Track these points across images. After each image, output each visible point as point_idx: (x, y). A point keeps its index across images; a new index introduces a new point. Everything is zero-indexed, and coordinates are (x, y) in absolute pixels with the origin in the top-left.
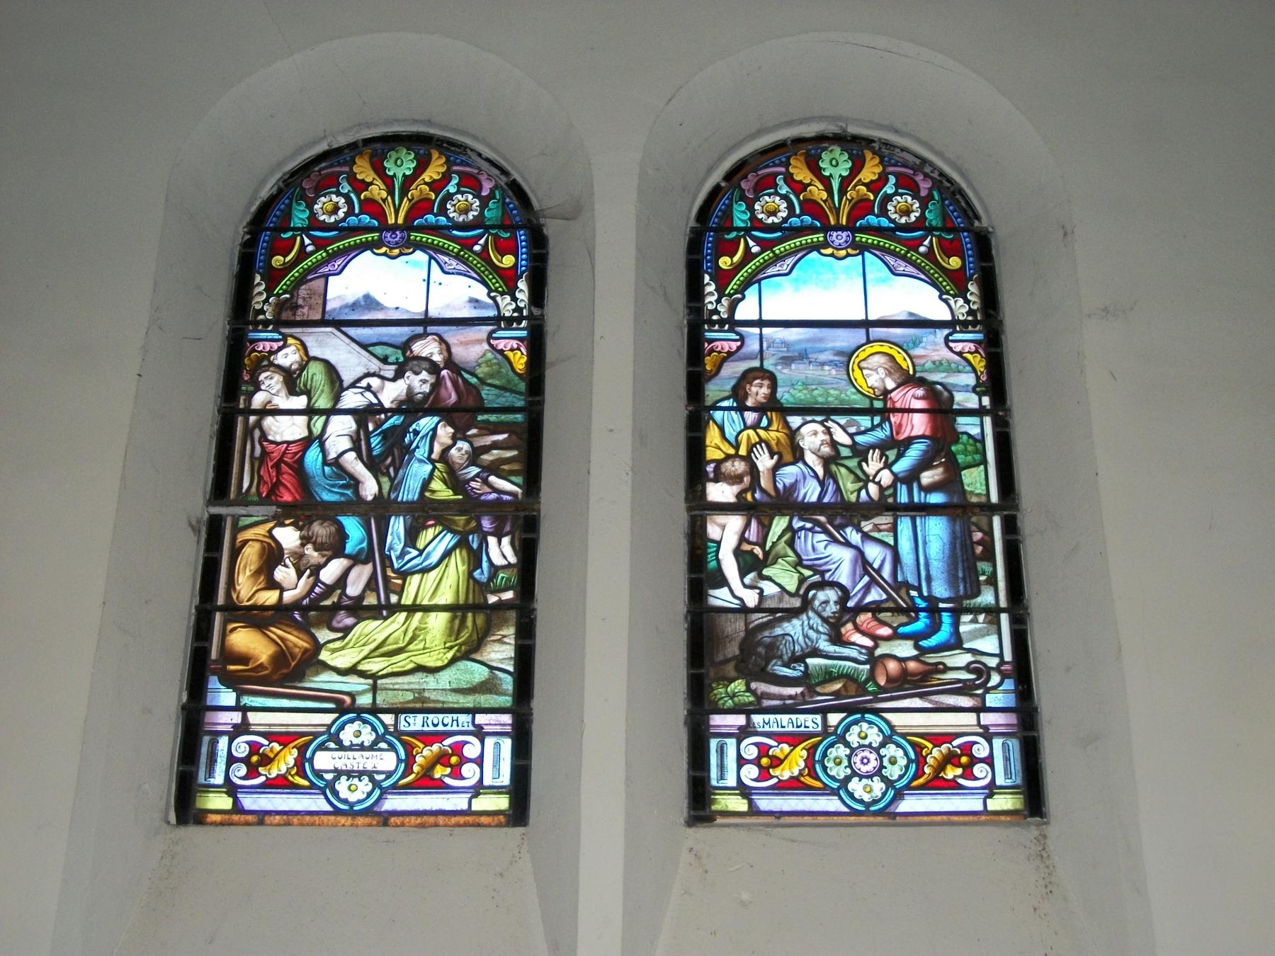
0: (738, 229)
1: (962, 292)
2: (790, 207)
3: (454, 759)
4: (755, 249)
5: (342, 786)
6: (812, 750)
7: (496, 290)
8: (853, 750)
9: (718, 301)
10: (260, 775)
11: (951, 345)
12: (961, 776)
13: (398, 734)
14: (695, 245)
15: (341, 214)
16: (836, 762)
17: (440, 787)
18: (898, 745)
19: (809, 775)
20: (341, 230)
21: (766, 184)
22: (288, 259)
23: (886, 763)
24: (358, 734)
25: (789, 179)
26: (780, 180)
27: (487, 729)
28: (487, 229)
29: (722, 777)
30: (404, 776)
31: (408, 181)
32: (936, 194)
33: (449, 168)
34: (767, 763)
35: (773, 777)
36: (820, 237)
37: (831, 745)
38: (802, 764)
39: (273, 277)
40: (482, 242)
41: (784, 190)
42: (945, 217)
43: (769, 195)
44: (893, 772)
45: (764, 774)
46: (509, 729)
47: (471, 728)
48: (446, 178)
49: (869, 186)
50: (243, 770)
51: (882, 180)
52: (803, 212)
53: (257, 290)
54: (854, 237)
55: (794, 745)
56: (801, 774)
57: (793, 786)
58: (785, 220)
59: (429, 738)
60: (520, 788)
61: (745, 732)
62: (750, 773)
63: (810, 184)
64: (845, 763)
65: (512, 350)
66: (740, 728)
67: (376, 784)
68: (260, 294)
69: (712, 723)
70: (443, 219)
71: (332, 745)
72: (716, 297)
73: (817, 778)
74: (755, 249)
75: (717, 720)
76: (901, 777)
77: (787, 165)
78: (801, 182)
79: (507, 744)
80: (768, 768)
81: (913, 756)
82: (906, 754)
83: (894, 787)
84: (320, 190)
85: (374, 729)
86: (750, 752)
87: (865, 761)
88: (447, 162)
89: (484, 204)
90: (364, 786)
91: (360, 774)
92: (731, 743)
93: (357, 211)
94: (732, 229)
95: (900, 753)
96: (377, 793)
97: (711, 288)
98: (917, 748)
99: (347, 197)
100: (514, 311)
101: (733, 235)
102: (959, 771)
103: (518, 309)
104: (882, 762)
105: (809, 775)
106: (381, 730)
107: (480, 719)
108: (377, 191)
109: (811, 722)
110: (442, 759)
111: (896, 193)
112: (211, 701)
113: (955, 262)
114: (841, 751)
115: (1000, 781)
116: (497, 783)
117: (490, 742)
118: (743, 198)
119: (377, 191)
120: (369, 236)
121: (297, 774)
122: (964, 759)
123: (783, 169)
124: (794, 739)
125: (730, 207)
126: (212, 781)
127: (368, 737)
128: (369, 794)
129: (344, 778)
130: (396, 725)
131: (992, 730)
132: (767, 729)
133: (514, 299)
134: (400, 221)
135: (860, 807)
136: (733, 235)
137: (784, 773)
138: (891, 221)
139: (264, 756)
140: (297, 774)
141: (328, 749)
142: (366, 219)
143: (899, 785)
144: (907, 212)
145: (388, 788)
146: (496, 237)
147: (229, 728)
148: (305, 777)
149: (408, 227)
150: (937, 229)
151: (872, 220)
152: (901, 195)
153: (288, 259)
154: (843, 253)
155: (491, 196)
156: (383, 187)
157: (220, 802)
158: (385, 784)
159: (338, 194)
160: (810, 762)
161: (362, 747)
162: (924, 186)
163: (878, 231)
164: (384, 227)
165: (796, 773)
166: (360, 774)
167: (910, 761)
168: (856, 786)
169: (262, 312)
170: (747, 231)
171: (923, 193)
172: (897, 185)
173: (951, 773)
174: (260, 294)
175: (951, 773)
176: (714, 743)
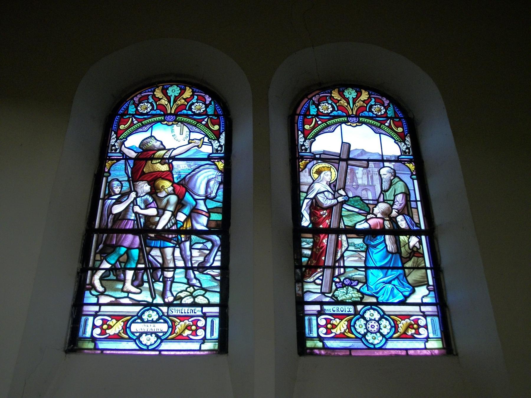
0: (130, 114)
1: (404, 141)
4: (135, 122)
6: (349, 321)
7: (212, 139)
8: (367, 321)
10: (332, 333)
13: (168, 316)
15: (149, 110)
16: (360, 326)
17: (188, 339)
18: (387, 319)
19: (349, 332)
22: (311, 126)
24: (149, 316)
25: (154, 96)
26: (150, 97)
30: (170, 334)
31: (176, 98)
32: (213, 103)
34: (329, 327)
37: (358, 319)
38: (345, 327)
40: (206, 120)
41: (151, 100)
42: (215, 110)
43: (323, 103)
44: (385, 331)
45: (329, 332)
46: (218, 314)
47: (200, 314)
48: (370, 98)
49: (364, 101)
52: (157, 109)
54: (359, 119)
55: (118, 321)
56: (119, 332)
59: (182, 318)
61: (319, 313)
62: (322, 331)
63: (162, 99)
64: (364, 327)
66: (318, 311)
67: (158, 337)
70: (190, 113)
73: (127, 334)
75: (86, 308)
76: (388, 333)
77: (331, 93)
79: (217, 321)
80: (106, 330)
81: (393, 324)
82: (390, 324)
85: (158, 313)
86: (322, 322)
88: (369, 94)
89: (207, 106)
90: (153, 338)
91: (151, 333)
93: (155, 109)
94: (310, 115)
96: (159, 341)
97: (302, 136)
100: (219, 146)
102: (190, 332)
104: (380, 326)
105: (349, 332)
106: (161, 314)
107: (205, 309)
108: (164, 102)
111: (375, 105)
112: (86, 301)
113: (400, 130)
115: (431, 335)
116: (213, 337)
117: (209, 320)
119: (164, 102)
120: (160, 118)
122: (415, 326)
123: (329, 95)
124: (341, 317)
125: (128, 107)
126: (311, 335)
127: (155, 317)
128: (155, 342)
129: (144, 335)
130: (168, 312)
131: (207, 314)
133: (219, 142)
134: (173, 112)
135: (145, 348)
137: (111, 332)
138: (192, 112)
139: (332, 324)
142: (158, 112)
143: (387, 337)
147: (93, 313)
148: (127, 334)
149: (176, 114)
151: (366, 113)
153: (311, 126)
154: (355, 124)
155: (210, 103)
158: (163, 338)
159: (148, 102)
160: (349, 327)
163: (187, 116)
164: (166, 114)
167: (392, 327)
168: (369, 337)
170: (133, 115)
172: (197, 99)
174: (114, 138)
175: (411, 332)
176: (307, 318)
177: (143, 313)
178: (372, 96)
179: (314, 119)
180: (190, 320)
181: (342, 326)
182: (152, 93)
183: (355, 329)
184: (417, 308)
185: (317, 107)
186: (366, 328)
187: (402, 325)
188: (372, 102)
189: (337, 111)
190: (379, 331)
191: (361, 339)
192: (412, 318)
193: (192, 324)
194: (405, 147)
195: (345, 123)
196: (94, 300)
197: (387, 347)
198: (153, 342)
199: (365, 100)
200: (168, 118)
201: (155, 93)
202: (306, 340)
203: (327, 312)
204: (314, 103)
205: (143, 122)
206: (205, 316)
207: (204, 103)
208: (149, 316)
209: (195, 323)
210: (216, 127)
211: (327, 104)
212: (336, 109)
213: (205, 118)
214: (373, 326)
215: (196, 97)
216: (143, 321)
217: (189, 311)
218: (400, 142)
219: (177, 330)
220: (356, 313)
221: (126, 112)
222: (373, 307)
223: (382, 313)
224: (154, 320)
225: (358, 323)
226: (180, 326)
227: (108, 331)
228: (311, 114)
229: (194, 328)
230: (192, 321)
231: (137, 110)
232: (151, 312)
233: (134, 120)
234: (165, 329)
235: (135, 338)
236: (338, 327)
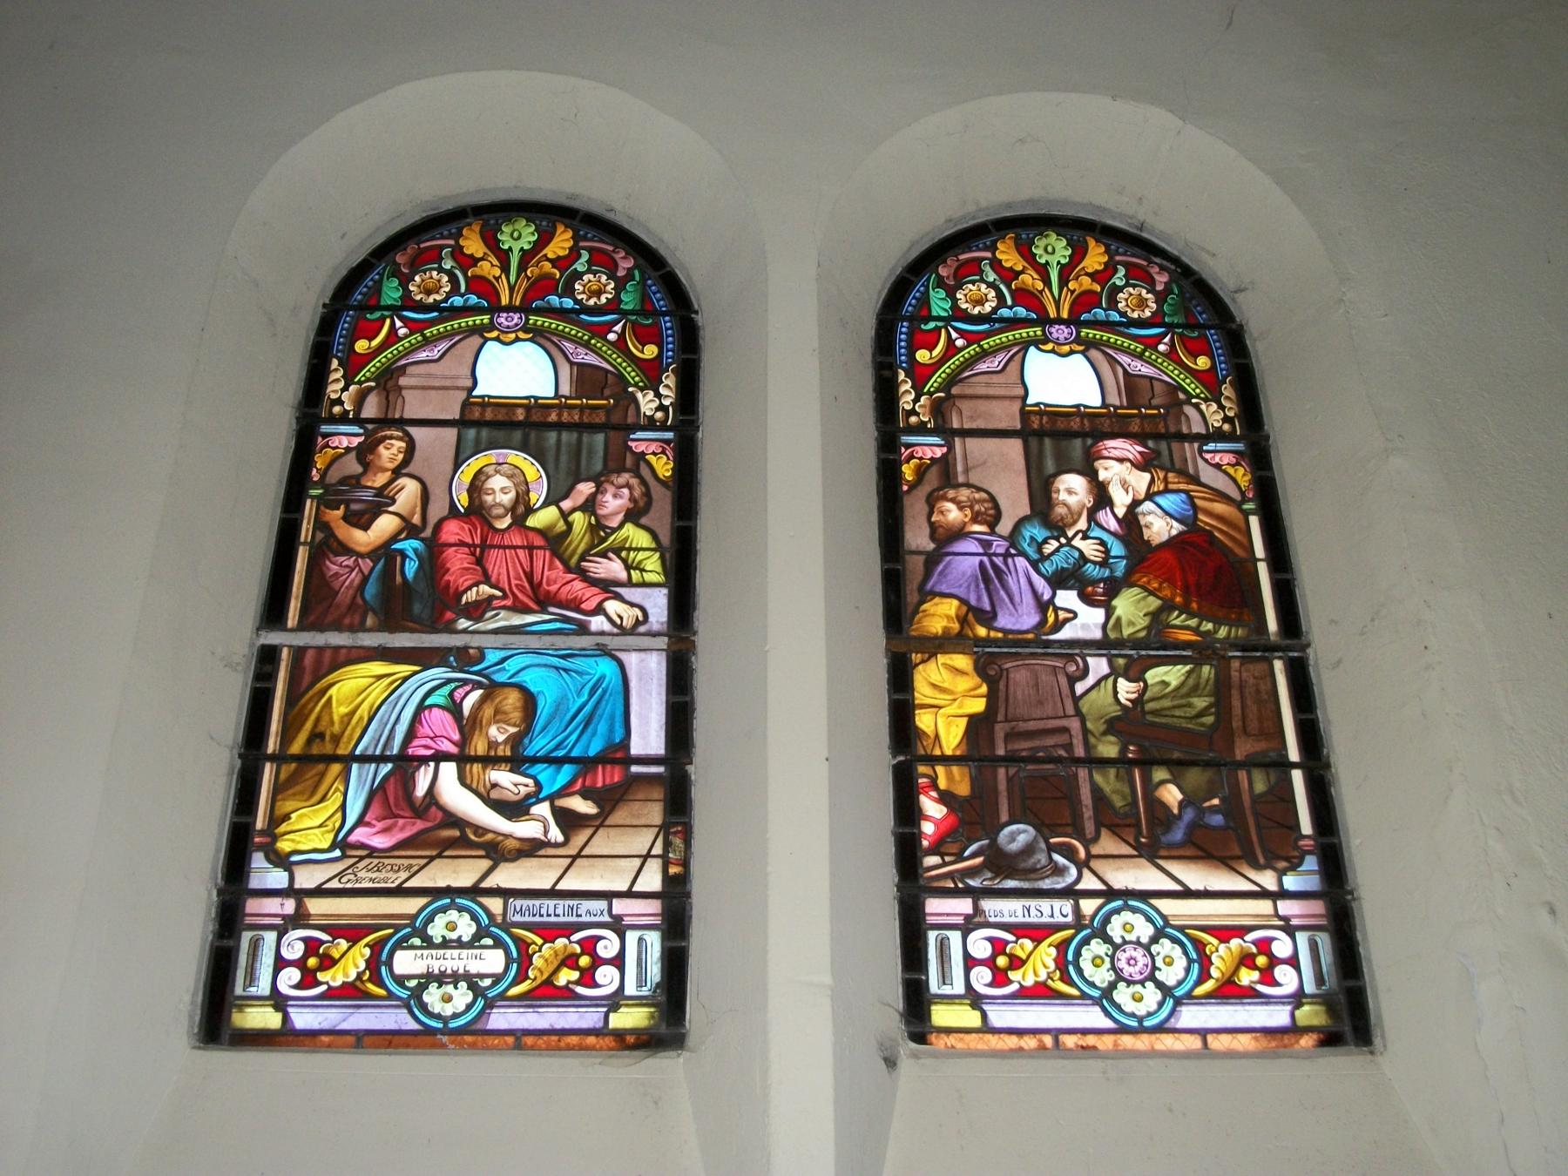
0: (939, 318)
2: (1000, 297)
3: (587, 962)
4: (960, 343)
5: (432, 997)
6: (1062, 947)
8: (1116, 947)
9: (916, 400)
10: (319, 984)
11: (1208, 456)
12: (577, 983)
13: (506, 926)
14: (327, 325)
16: (1094, 967)
17: (1249, 994)
18: (1175, 940)
20: (441, 310)
21: (972, 269)
22: (935, 353)
23: (1159, 963)
25: (996, 265)
27: (627, 921)
28: (624, 314)
29: (945, 978)
30: (515, 983)
31: (527, 257)
32: (637, 273)
33: (1111, 258)
35: (321, 983)
36: (486, 319)
38: (362, 966)
39: (920, 375)
41: (991, 277)
42: (645, 298)
43: (973, 283)
44: (1169, 976)
45: (1000, 978)
46: (1323, 922)
47: (606, 918)
48: (574, 254)
49: (555, 262)
50: (293, 974)
51: (1110, 269)
52: (469, 290)
53: (903, 388)
54: (1078, 333)
55: (1038, 941)
56: (359, 976)
57: (1040, 993)
58: (995, 310)
60: (672, 993)
64: (1107, 964)
65: (654, 454)
66: (968, 918)
68: (337, 380)
69: (928, 909)
71: (417, 941)
72: (913, 396)
73: (381, 984)
74: (960, 343)
75: (252, 905)
76: (1180, 983)
77: (993, 248)
78: (472, 256)
79: (654, 940)
83: (1173, 996)
84: (417, 264)
85: (474, 918)
86: (981, 949)
87: (1131, 961)
88: (1107, 251)
90: (462, 996)
92: (955, 937)
94: (930, 318)
95: (1177, 952)
96: (480, 1003)
97: (908, 386)
98: (1199, 945)
99: (450, 274)
100: (657, 409)
101: (931, 325)
102: (575, 975)
103: (661, 408)
106: (485, 920)
107: (619, 906)
108: (489, 268)
109: (1061, 910)
110: (1247, 960)
111: (1127, 285)
112: (255, 882)
113: (1203, 362)
114: (1097, 947)
115: (631, 989)
118: (396, 273)
120: (478, 319)
121: (370, 980)
122: (1263, 959)
123: (989, 255)
124: (1038, 933)
126: (947, 990)
127: (466, 928)
128: (469, 1007)
129: (433, 987)
131: (1294, 922)
132: (998, 919)
134: (1065, 315)
135: (1133, 1023)
136: (931, 325)
137: (1022, 978)
138: (577, 302)
140: (370, 980)
141: (413, 947)
143: (1179, 993)
144: (980, 302)
145: (1182, 997)
146: (635, 325)
147: (960, 920)
148: (381, 984)
150: (1178, 326)
152: (1134, 286)
154: (1067, 348)
156: (495, 262)
157: (263, 1018)
159: (440, 270)
160: (1061, 963)
161: (460, 944)
162: (1161, 280)
163: (560, 313)
164: (1044, 321)
165: (352, 976)
166: (455, 978)
168: (1122, 995)
169: (913, 412)
170: (395, 310)
171: (621, 273)
173: (1247, 977)
174: (337, 380)
176: (932, 936)
177: (430, 919)
178: (1118, 258)
179: (388, 322)
180: (575, 937)
181: (1041, 962)
182: (452, 242)
183: (1080, 971)
184: (1265, 906)
185: (951, 293)
186: (1113, 968)
187: (1222, 956)
188: (1119, 279)
189: (1011, 308)
190: (1152, 977)
191: (1097, 1002)
192: (1251, 937)
193: (578, 949)
194: (1220, 416)
195: (1037, 343)
196: (278, 879)
197: (1179, 1025)
198: (462, 1008)
199: (1097, 272)
200: (502, 319)
201: (462, 242)
202: (930, 1003)
203: (992, 920)
204: (940, 283)
205: (427, 332)
206: (618, 926)
207: (612, 276)
208: (452, 926)
209: (589, 945)
210: (650, 351)
211: (983, 286)
212: (1009, 302)
213: (616, 322)
214: (1133, 962)
215: (585, 256)
216: (428, 943)
217: (551, 911)
218: (1206, 400)
219: (1214, 972)
220: (1079, 922)
221: (373, 302)
222: (1131, 903)
223: (1160, 922)
224: (465, 939)
225: (1086, 954)
226: (544, 955)
227: (320, 976)
228: (934, 313)
229: (584, 961)
230: (578, 942)
231: (407, 293)
232: (453, 915)
233: (398, 324)
234: (498, 967)
235: (403, 994)
236: (1029, 965)
